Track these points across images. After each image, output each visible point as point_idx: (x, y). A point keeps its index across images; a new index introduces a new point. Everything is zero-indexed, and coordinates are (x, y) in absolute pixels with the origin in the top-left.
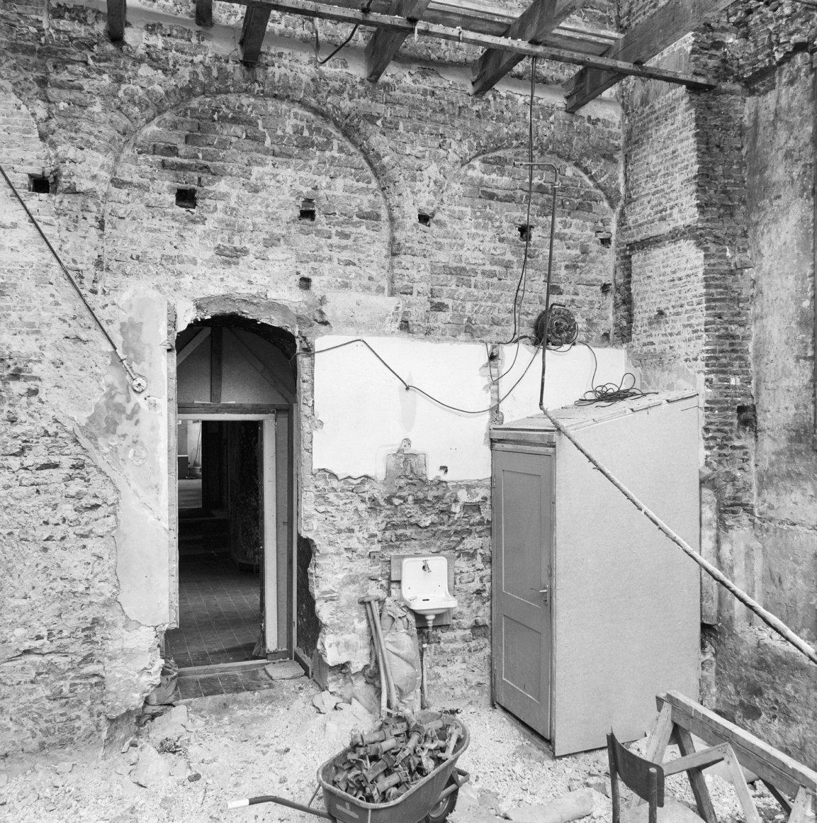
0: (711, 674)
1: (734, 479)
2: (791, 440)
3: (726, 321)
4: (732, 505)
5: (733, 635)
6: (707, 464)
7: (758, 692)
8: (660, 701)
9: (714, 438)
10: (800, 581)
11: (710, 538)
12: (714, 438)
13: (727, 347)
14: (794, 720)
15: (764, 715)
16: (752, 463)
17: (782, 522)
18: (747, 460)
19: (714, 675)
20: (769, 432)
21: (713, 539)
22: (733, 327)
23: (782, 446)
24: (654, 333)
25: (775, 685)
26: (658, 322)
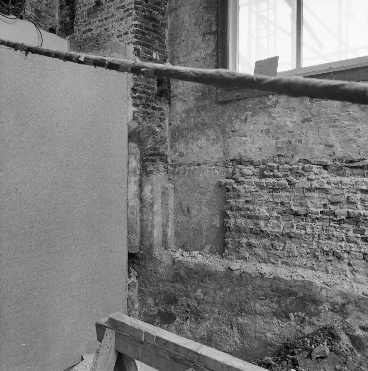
0: (135, 293)
1: (154, 133)
2: (198, 99)
3: (150, 6)
4: (152, 155)
5: (152, 258)
6: (135, 118)
7: (173, 300)
8: (100, 329)
9: (140, 98)
10: (205, 208)
11: (135, 182)
12: (140, 98)
13: (150, 27)
14: (203, 318)
15: (178, 319)
16: (167, 122)
17: (190, 165)
18: (164, 119)
19: (137, 293)
20: (180, 97)
21: (137, 184)
22: (156, 12)
23: (190, 105)
24: (92, 21)
25: (188, 293)
26: (96, 11)
